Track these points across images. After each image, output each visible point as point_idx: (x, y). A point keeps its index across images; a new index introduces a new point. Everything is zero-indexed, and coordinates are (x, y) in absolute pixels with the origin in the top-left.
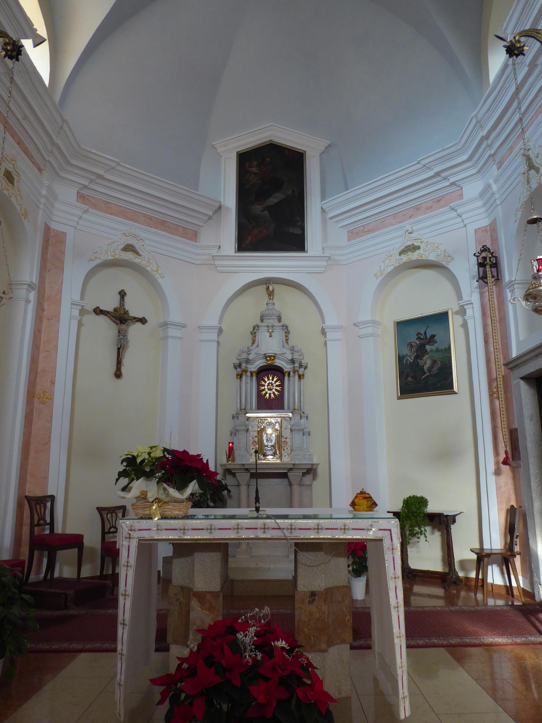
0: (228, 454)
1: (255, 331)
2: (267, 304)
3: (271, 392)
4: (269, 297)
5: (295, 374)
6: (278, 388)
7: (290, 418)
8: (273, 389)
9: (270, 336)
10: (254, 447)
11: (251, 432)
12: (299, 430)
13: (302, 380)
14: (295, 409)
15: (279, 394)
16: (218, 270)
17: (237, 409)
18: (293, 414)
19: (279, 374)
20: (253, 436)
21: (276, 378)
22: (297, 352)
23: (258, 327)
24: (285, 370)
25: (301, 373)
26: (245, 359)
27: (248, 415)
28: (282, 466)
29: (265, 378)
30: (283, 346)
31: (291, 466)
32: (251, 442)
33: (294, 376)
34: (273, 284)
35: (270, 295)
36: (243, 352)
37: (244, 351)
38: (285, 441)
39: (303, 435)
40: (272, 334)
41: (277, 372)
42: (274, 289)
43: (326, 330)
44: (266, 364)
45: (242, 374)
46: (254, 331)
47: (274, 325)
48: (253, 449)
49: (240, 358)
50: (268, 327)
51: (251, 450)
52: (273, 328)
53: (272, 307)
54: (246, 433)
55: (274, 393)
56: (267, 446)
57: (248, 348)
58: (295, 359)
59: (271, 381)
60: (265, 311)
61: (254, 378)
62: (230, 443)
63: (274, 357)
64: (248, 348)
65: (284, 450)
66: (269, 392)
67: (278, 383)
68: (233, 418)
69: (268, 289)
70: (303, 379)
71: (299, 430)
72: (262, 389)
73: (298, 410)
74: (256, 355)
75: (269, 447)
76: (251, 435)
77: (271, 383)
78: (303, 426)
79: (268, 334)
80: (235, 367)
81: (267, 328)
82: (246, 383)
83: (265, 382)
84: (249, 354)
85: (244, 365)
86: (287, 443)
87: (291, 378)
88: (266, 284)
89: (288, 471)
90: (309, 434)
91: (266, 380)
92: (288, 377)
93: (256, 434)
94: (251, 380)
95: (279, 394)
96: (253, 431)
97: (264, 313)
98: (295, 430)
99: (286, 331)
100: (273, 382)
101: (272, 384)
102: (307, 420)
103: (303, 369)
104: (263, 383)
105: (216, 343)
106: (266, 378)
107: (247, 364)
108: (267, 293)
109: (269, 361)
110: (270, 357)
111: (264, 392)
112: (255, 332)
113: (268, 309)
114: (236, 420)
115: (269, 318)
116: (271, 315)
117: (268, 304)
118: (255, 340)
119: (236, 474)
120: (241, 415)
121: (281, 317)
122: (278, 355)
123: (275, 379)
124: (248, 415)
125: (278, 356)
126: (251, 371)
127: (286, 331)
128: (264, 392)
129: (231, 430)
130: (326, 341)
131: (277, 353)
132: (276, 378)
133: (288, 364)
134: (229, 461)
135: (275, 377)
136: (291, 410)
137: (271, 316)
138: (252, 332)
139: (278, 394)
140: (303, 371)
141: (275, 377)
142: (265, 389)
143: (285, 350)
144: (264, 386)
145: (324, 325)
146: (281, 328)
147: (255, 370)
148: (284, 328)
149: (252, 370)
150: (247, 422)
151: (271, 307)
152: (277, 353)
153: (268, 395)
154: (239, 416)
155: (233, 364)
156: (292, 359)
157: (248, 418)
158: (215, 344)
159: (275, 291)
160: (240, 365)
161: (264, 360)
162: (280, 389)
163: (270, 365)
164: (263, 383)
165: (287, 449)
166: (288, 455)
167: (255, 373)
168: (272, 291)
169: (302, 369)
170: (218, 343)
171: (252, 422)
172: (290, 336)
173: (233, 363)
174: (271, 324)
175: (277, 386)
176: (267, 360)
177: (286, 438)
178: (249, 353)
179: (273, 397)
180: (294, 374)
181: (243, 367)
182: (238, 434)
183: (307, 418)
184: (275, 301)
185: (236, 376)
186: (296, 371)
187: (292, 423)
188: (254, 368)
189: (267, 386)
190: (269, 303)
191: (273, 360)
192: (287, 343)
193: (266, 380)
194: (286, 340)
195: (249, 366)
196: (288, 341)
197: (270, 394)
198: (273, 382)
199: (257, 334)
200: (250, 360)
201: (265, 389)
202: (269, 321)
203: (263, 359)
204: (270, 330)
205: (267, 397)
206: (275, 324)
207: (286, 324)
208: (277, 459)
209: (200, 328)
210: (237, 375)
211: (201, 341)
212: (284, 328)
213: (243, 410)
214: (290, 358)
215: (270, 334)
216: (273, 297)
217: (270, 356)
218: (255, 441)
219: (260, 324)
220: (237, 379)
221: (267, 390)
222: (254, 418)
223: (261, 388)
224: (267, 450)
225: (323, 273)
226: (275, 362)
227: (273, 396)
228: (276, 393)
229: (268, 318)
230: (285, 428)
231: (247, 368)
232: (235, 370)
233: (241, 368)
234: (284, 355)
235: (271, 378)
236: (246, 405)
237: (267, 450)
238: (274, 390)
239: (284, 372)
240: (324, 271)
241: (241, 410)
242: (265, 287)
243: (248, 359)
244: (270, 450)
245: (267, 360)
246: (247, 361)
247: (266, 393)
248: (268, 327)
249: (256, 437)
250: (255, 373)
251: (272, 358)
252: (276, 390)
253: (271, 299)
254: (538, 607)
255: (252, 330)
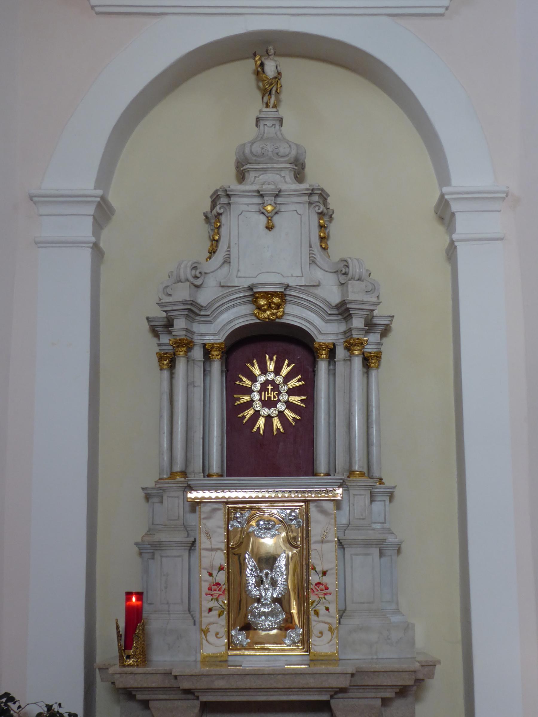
0: (122, 632)
1: (217, 209)
2: (258, 120)
3: (273, 412)
4: (266, 99)
5: (351, 355)
6: (295, 399)
7: (338, 504)
8: (279, 401)
9: (270, 228)
10: (214, 604)
11: (204, 553)
12: (367, 544)
13: (373, 373)
14: (351, 473)
15: (298, 418)
16: (93, 7)
17: (161, 471)
18: (348, 490)
19: (300, 353)
20: (212, 567)
21: (288, 365)
22: (359, 279)
23: (228, 196)
24: (320, 339)
25: (370, 348)
26: (184, 302)
27: (193, 495)
28: (312, 682)
29: (253, 365)
30: (313, 261)
31: (344, 683)
32: (205, 586)
33: (349, 359)
34: (276, 58)
35: (266, 92)
36: (180, 281)
37: (183, 277)
38: (319, 584)
39: (381, 555)
40: (276, 219)
41: (292, 347)
42: (279, 73)
43: (454, 207)
44: (257, 321)
45: (174, 354)
46: (214, 212)
47: (280, 191)
48: (210, 610)
49: (170, 299)
50: (262, 196)
51: (205, 614)
52: (280, 200)
53: (272, 130)
54: (187, 552)
55: (281, 414)
56: (258, 601)
57: (195, 268)
58: (351, 302)
59: (271, 377)
60: (252, 143)
61: (216, 367)
62: (129, 595)
63: (283, 296)
64: (195, 268)
65: (317, 613)
66: (265, 411)
67: (294, 383)
68: (148, 497)
69: (260, 71)
70: (378, 368)
71: (367, 544)
72: (242, 401)
73: (362, 474)
74: (221, 292)
75: (264, 605)
76: (205, 562)
77: (272, 382)
78: (378, 526)
79: (263, 220)
80: (155, 331)
81: (258, 200)
82: (189, 384)
83: (254, 379)
84: (197, 287)
85: (180, 324)
86: (327, 588)
87: (340, 367)
88: (255, 55)
89: (332, 697)
90: (399, 551)
91: (256, 371)
92: (329, 364)
93: (220, 559)
94: (206, 373)
95: (298, 418)
96: (212, 550)
97: (247, 151)
98: (354, 543)
99: (322, 208)
100: (279, 379)
101: (276, 387)
102: (391, 501)
103: (378, 336)
104: (247, 382)
105: (90, 250)
106: (256, 366)
107: (193, 320)
108: (259, 88)
109: (265, 311)
110: (268, 295)
111: (249, 413)
112: (220, 214)
113: (261, 138)
114: (157, 505)
115: (265, 166)
116: (271, 159)
117: (261, 123)
118: (217, 241)
119: (151, 704)
120: (172, 494)
121: (303, 166)
122: (294, 288)
123: (285, 371)
124: (193, 495)
125: (293, 293)
126: (204, 345)
127: (322, 208)
128: (249, 413)
129: (139, 540)
130: (452, 242)
131: (291, 284)
132: (288, 365)
133: (327, 321)
134: (128, 657)
135: (286, 362)
136: (340, 476)
137: (271, 160)
138: (209, 215)
139: (294, 419)
140: (377, 344)
141: (286, 362)
142: (252, 401)
143: (319, 275)
144: (249, 391)
145: (445, 190)
146: (306, 199)
147: (220, 339)
148: (315, 198)
149: (210, 340)
150: (191, 519)
151: (269, 130)
152: (292, 282)
153: (261, 422)
154: (165, 497)
155: (146, 322)
156: (343, 303)
157: (195, 504)
158: (86, 255)
159: (283, 81)
160: (169, 324)
161: (248, 309)
162: (302, 401)
163: (269, 323)
164: (247, 382)
165: (327, 609)
166: (330, 630)
167: (219, 349)
168: (276, 78)
169: (374, 338)
170: (96, 248)
171: (207, 518)
172: (333, 229)
173: (148, 319)
174: (272, 187)
175: (291, 392)
176: (259, 308)
177: (324, 573)
178: (198, 282)
179: (278, 429)
180: (348, 354)
181: (179, 330)
182: (162, 557)
183: (391, 496)
184: (283, 111)
185: (156, 359)
186: (356, 345)
187: (343, 520)
188: (214, 334)
189: (260, 392)
190: (264, 119)
191: (278, 306)
192: (325, 249)
193: (256, 371)
194: (322, 239)
195: (199, 328)
196: (327, 244)
197: (269, 418)
198: (279, 379)
199: (223, 218)
200: (201, 308)
201: (252, 401)
202: (263, 177)
203: (246, 303)
204: (269, 208)
205: (259, 428)
206: (284, 187)
207: (323, 186)
208: (294, 643)
209: (35, 199)
210: (161, 357)
211: (36, 243)
212: (315, 198)
213: (179, 478)
214: (335, 299)
215: (269, 219)
216: (278, 100)
217: (267, 293)
218: (218, 584)
219: (235, 186)
220: (161, 369)
221: (258, 405)
222: (216, 506)
223: (239, 399)
224: (260, 615)
225: (442, 15)
226: (284, 313)
227: (279, 426)
228: (289, 414)
229: (261, 166)
230: (319, 538)
231: (193, 333)
232: (155, 340)
233: (170, 333)
234: (318, 291)
235: (271, 367)
236: (187, 461)
237: (260, 615)
238: (281, 406)
239: (316, 346)
240: (447, 8)
241: (173, 475)
242: (250, 65)
243: (194, 303)
244: (272, 613)
245: (259, 308)
246: (190, 310)
247: (257, 415)
248: (262, 196)
249: (221, 569)
250: (219, 349)
251: (276, 300)
252: (290, 405)
253: (271, 105)
254: (360, 345)
255: (208, 208)
